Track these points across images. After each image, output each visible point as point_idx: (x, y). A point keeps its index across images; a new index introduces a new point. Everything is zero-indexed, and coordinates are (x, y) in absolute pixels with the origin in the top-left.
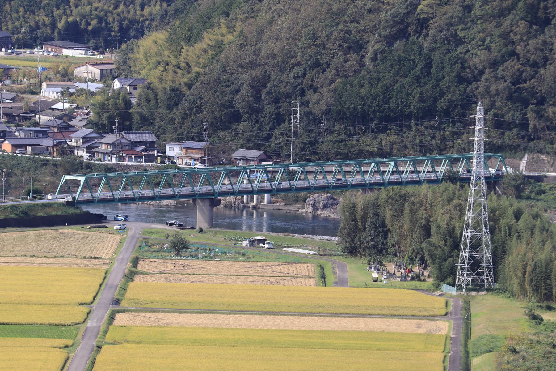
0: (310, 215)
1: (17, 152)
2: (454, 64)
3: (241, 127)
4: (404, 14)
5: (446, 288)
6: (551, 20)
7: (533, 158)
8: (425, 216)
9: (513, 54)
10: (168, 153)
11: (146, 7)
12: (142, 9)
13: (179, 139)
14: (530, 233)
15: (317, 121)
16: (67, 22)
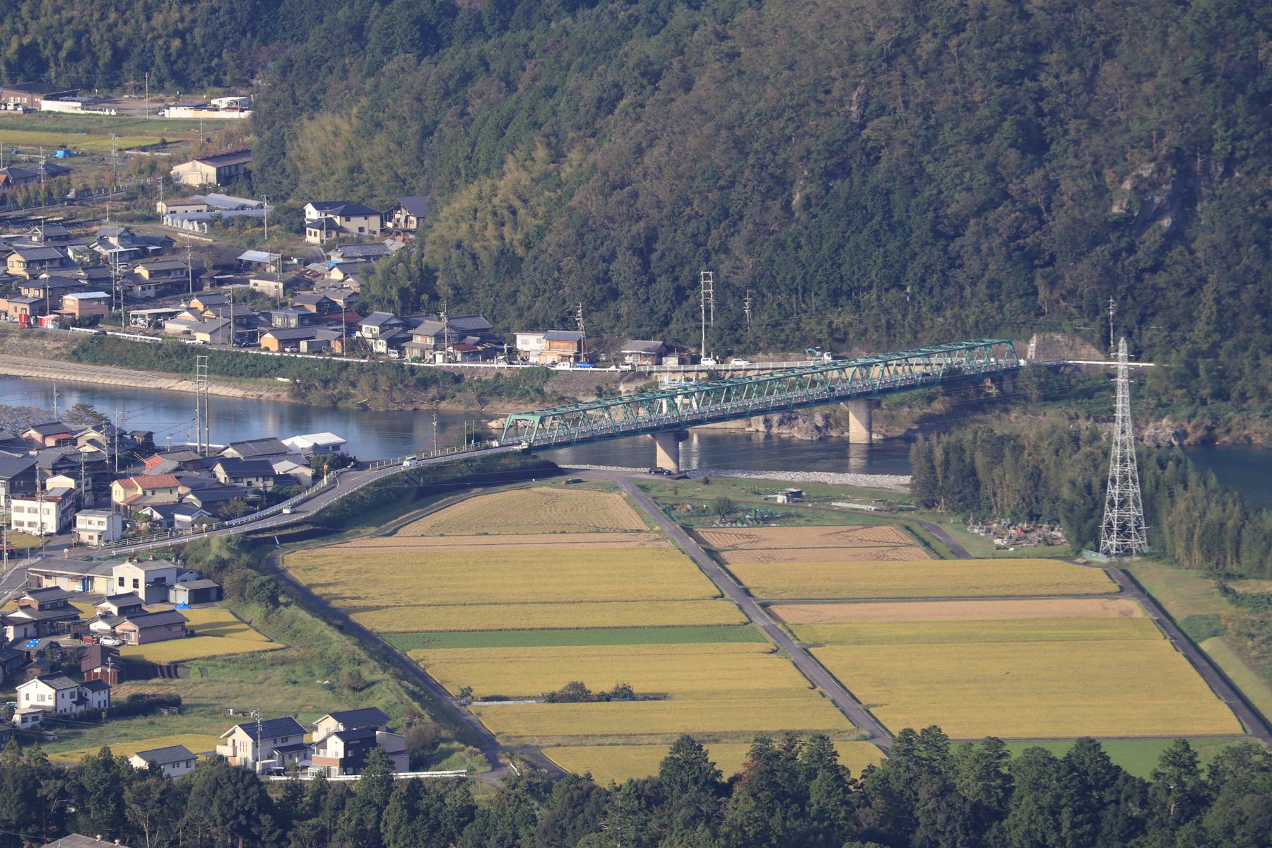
0: (762, 436)
1: (287, 350)
2: (925, 213)
3: (624, 308)
4: (843, 141)
5: (1089, 555)
6: (1049, 145)
7: (1044, 339)
8: (1031, 464)
9: (1006, 195)
10: (519, 346)
11: (155, 14)
12: (149, 19)
13: (532, 327)
14: (1182, 486)
15: (739, 295)
16: (21, 45)
